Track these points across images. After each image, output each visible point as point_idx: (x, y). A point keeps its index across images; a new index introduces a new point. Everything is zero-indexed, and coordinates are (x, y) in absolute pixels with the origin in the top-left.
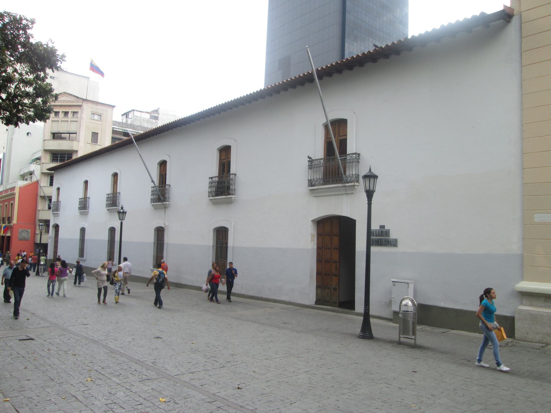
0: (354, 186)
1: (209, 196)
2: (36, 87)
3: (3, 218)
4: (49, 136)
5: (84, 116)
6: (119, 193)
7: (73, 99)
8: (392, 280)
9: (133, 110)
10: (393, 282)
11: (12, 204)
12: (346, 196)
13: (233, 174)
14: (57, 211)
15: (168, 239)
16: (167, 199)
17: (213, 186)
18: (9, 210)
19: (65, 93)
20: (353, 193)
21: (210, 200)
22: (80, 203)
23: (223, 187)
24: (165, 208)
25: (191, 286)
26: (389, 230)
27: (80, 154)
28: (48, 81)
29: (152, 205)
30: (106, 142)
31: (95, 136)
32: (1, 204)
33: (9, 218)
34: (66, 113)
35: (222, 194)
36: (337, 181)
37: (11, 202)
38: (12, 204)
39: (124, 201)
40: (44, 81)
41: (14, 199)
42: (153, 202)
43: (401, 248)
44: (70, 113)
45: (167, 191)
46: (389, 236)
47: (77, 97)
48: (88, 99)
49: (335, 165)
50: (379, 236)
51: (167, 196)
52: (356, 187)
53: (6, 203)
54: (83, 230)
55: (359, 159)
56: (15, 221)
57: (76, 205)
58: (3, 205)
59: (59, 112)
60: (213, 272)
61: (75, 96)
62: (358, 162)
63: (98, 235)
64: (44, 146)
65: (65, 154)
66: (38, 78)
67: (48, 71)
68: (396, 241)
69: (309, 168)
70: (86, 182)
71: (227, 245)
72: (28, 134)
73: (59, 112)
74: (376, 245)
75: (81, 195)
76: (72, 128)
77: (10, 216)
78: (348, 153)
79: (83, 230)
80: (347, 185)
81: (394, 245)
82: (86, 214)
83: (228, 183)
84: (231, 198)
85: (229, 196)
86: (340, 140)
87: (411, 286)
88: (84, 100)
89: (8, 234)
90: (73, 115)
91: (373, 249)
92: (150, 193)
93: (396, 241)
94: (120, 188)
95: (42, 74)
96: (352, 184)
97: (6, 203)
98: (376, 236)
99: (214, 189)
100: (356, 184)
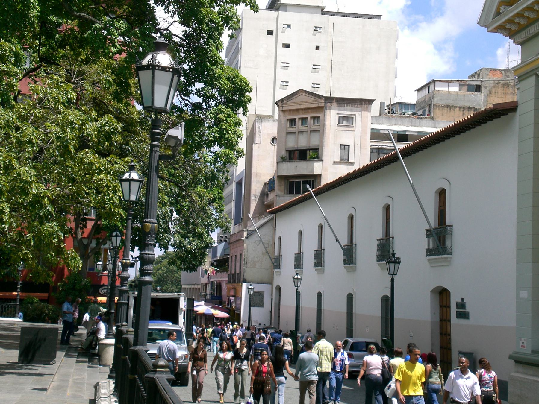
6: (356, 244)
7: (312, 99)
9: (434, 81)
27: (325, 181)
30: (361, 159)
34: (304, 120)
36: (8, 314)
39: (399, 249)
51: (448, 244)
59: (295, 119)
60: (153, 308)
64: (277, 171)
70: (300, 233)
76: (314, 142)
78: (447, 224)
82: (354, 270)
91: (251, 308)
92: (375, 248)
94: (356, 240)
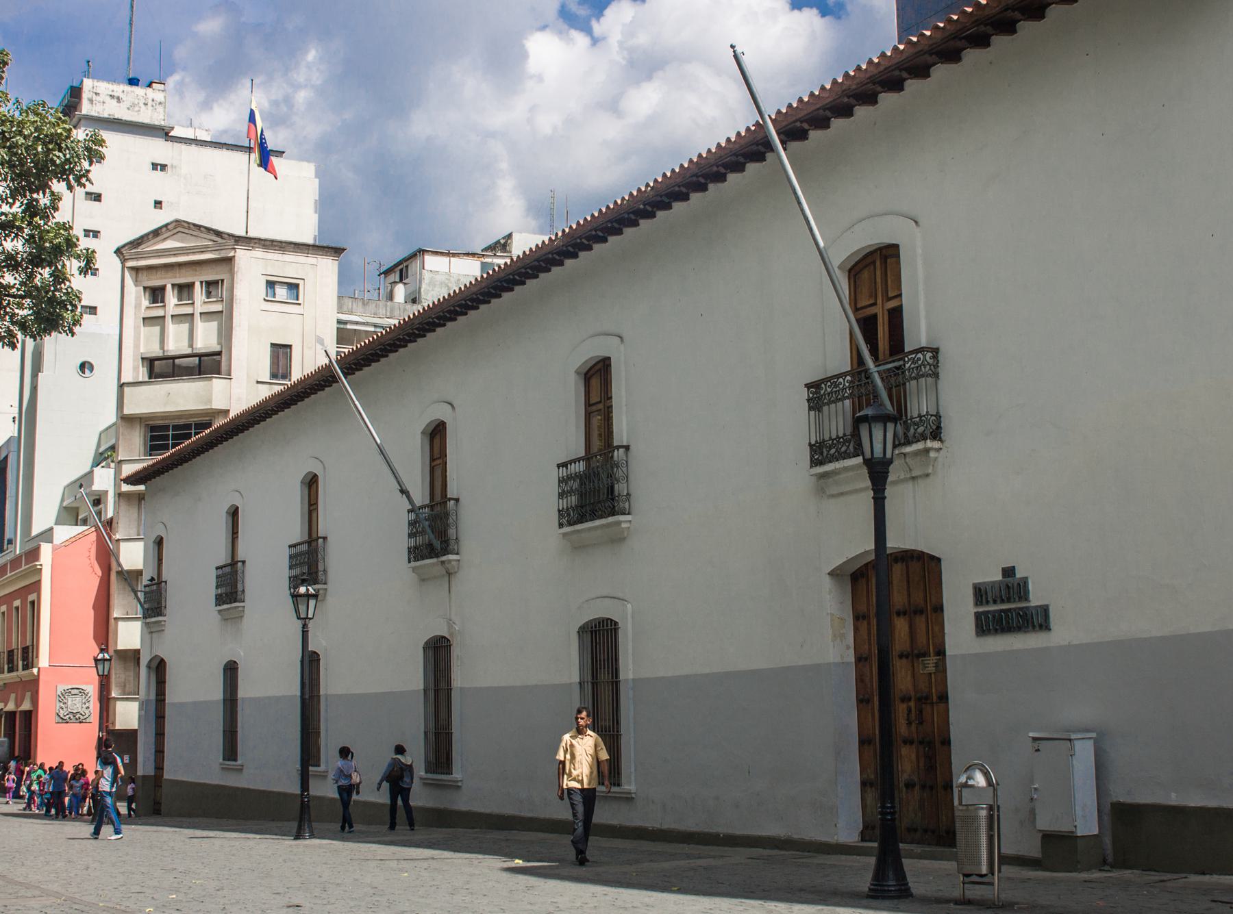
0: (927, 451)
1: (561, 525)
2: (32, 236)
3: (11, 653)
4: (134, 370)
5: (241, 291)
6: (325, 538)
8: (1031, 734)
10: (1035, 739)
11: (33, 603)
12: (910, 484)
13: (618, 447)
14: (160, 614)
15: (466, 675)
16: (453, 546)
17: (571, 492)
18: (24, 623)
19: (178, 223)
20: (928, 475)
21: (565, 535)
22: (294, 561)
23: (595, 491)
24: (449, 574)
25: (531, 819)
26: (1025, 581)
28: (61, 217)
29: (414, 569)
31: (281, 352)
32: (4, 608)
33: (25, 650)
34: (185, 290)
35: (594, 516)
37: (32, 597)
38: (33, 603)
40: (46, 217)
41: (36, 586)
42: (416, 559)
43: (1061, 634)
44: (198, 285)
45: (619, 473)
46: (1027, 599)
47: (218, 233)
48: (251, 234)
49: (879, 396)
50: (1003, 601)
52: (932, 454)
53: (17, 603)
54: (231, 670)
55: (936, 366)
56: (44, 660)
57: (209, 588)
58: (9, 609)
61: (209, 230)
62: (936, 375)
63: (271, 680)
65: (166, 428)
66: (32, 210)
67: (58, 186)
68: (1045, 610)
69: (810, 408)
71: (617, 676)
72: (83, 366)
73: (163, 288)
74: (996, 631)
75: (296, 533)
77: (28, 643)
79: (231, 670)
80: (908, 449)
81: (1041, 626)
83: (610, 476)
84: (619, 523)
85: (610, 519)
86: (889, 311)
87: (1084, 752)
88: (238, 240)
89: (26, 706)
90: (209, 294)
92: (213, 582)
93: (1045, 610)
95: (44, 200)
96: (919, 446)
97: (17, 603)
98: (995, 602)
99: (573, 500)
100: (929, 444)
